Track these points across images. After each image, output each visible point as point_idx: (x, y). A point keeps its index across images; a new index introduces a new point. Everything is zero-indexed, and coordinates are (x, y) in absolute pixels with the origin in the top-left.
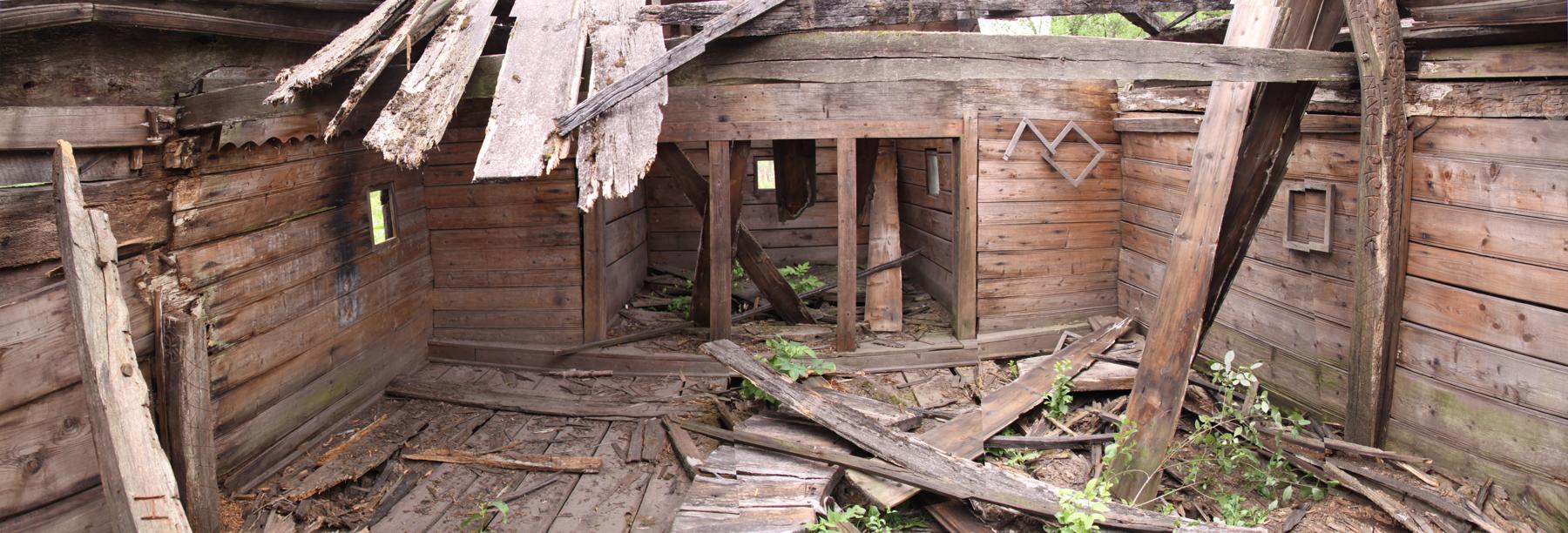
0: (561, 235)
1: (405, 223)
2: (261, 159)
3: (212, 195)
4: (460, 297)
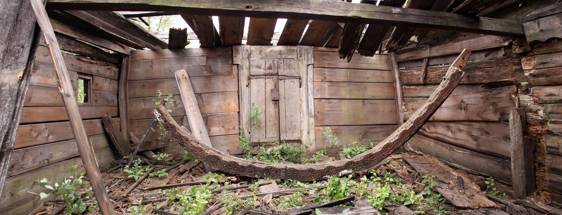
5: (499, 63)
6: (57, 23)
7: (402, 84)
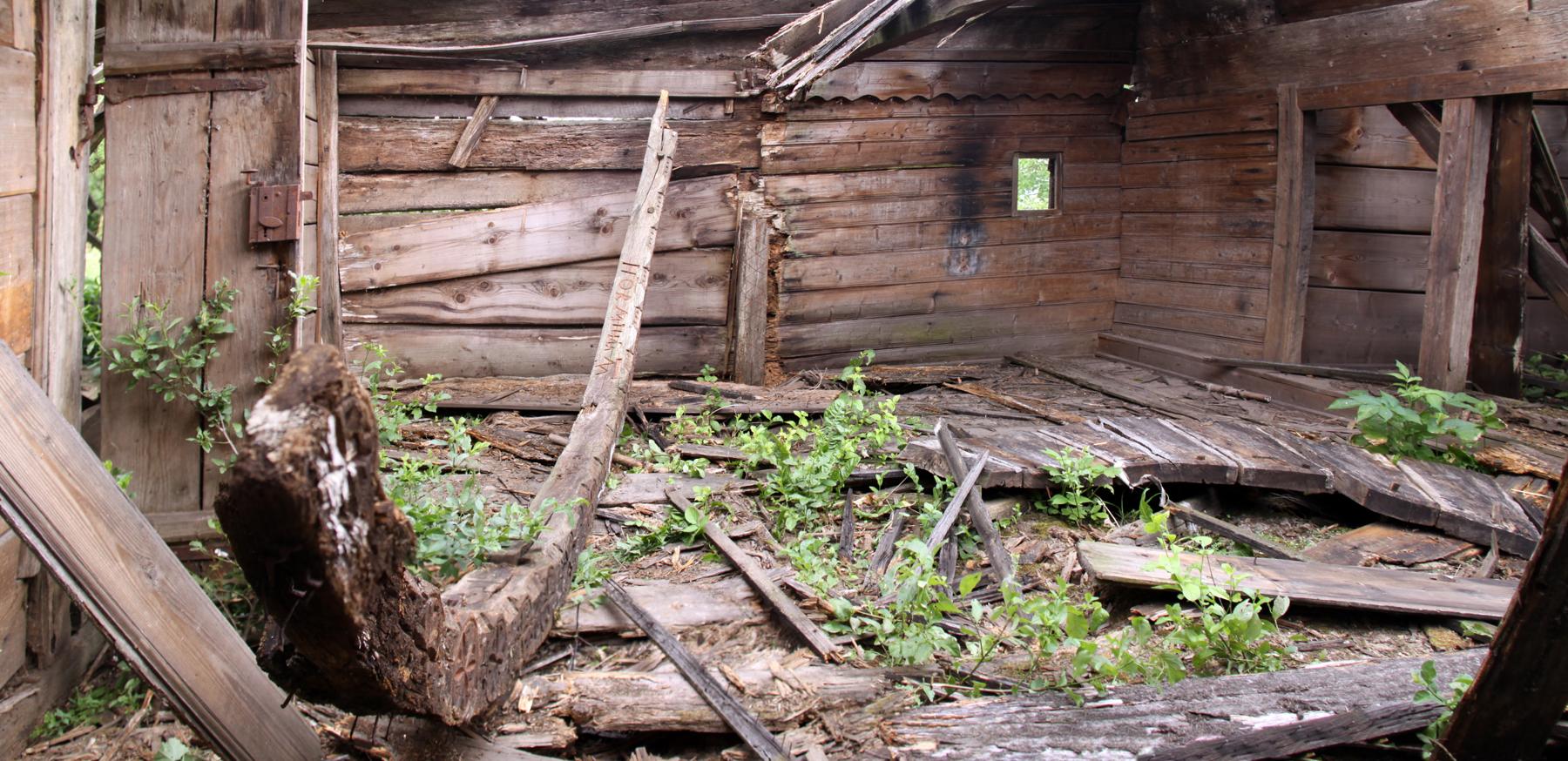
0: (1254, 224)
1: (1070, 198)
2: (853, 113)
3: (797, 137)
4: (1142, 290)
5: (716, 128)
6: (614, 69)
7: (345, 170)
